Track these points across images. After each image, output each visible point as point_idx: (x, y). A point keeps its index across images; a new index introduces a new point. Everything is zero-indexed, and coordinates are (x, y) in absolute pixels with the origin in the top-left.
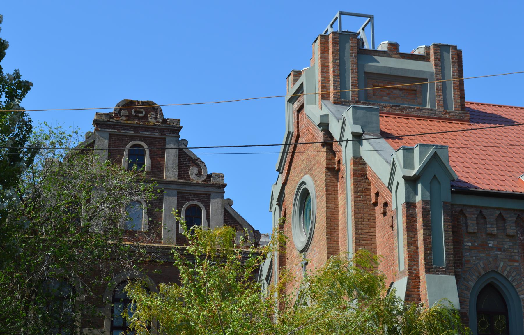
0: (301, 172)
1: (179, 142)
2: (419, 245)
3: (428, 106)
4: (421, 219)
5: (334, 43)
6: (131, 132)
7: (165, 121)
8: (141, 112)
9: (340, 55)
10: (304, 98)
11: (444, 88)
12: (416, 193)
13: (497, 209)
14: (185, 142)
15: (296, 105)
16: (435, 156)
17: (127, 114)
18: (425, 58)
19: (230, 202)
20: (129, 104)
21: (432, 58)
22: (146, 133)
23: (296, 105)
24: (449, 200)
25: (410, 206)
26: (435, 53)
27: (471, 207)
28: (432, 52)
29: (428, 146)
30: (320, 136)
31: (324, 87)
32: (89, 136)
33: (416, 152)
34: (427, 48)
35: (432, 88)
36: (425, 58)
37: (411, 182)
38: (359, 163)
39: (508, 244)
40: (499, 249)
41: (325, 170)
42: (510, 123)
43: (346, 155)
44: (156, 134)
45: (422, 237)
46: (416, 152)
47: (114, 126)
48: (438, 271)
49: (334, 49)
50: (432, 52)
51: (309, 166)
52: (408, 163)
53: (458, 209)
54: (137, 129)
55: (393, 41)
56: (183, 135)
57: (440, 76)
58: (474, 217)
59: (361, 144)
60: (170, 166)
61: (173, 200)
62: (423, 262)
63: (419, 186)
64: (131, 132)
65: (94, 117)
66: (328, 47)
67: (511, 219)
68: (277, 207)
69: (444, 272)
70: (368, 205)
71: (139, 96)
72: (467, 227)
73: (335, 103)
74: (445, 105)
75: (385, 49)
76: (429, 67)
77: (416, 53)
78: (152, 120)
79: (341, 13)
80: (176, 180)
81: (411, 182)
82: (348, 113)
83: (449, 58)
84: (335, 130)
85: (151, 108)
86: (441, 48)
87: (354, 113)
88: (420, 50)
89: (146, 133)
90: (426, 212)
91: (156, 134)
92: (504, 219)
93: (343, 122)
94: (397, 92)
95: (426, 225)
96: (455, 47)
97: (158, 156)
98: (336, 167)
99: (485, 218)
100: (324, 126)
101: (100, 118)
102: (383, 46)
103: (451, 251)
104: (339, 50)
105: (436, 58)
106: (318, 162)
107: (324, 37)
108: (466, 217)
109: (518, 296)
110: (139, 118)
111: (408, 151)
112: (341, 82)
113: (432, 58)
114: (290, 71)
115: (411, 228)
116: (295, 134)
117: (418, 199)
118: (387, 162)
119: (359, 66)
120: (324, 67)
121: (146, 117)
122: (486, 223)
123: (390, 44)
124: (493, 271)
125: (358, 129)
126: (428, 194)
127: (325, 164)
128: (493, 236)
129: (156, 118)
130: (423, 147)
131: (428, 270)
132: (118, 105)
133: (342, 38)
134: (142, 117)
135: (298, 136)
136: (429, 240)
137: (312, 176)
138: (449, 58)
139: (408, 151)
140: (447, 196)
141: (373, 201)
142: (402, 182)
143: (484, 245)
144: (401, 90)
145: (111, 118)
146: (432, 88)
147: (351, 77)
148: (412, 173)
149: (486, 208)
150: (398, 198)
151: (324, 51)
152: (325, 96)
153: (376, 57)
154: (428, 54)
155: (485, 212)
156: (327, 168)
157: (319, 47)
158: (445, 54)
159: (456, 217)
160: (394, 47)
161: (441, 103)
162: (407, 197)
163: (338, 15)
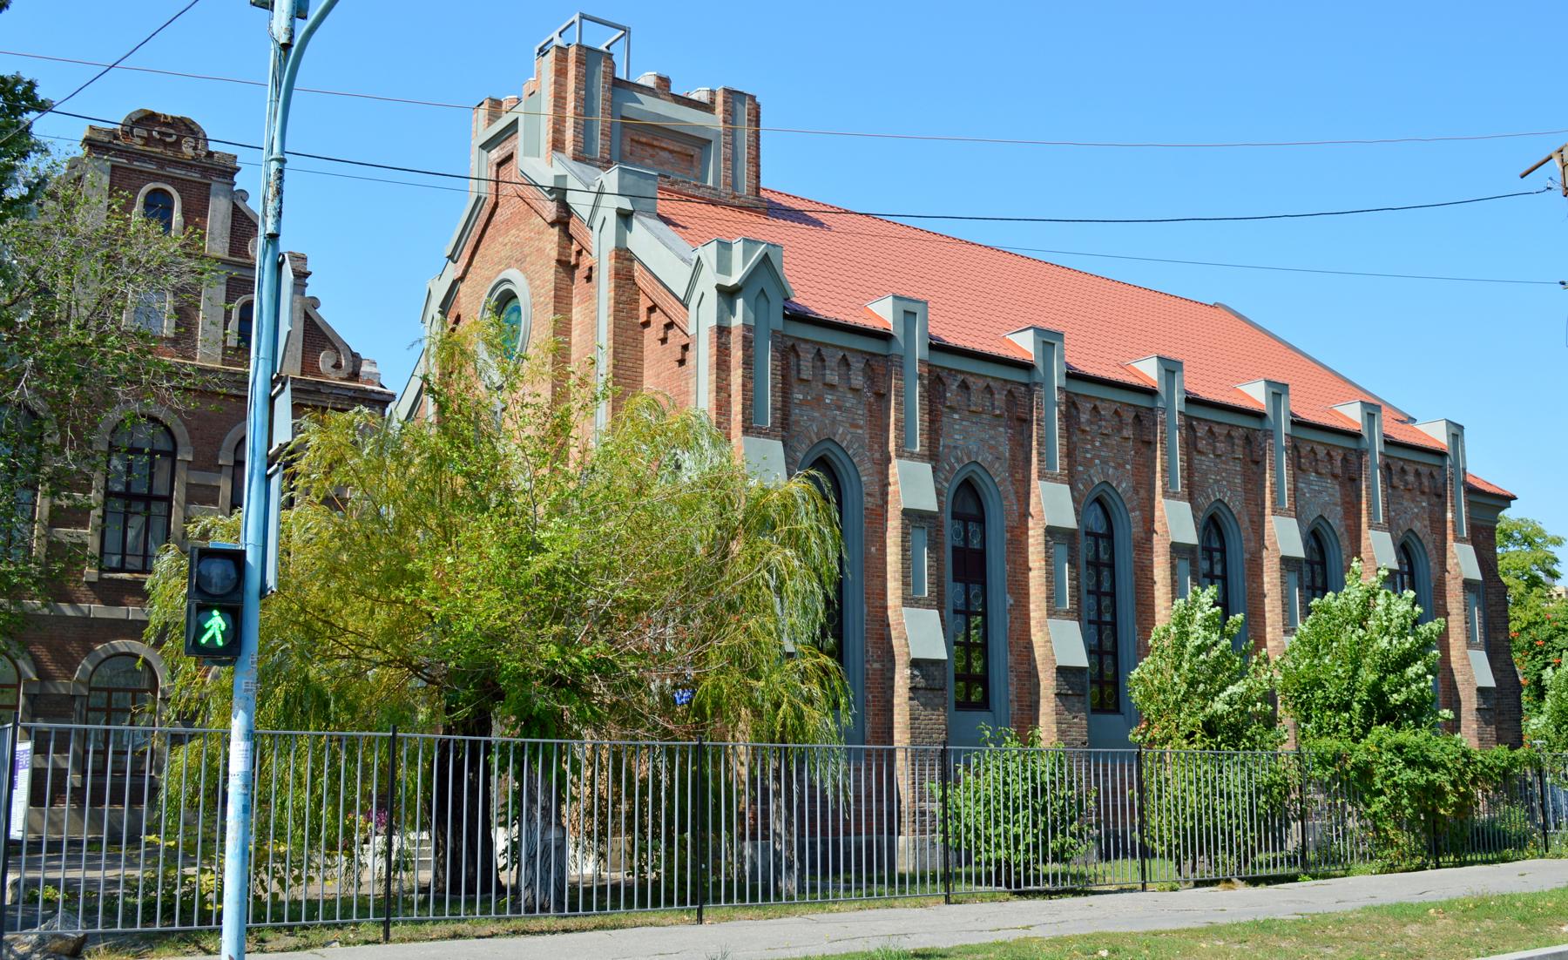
0: (500, 263)
1: (233, 193)
2: (733, 392)
3: (710, 183)
4: (740, 353)
5: (579, 62)
6: (151, 167)
7: (210, 154)
8: (170, 135)
9: (585, 81)
10: (519, 143)
11: (733, 159)
12: (733, 312)
13: (841, 348)
14: (244, 195)
15: (496, 154)
16: (765, 259)
17: (145, 134)
18: (707, 107)
19: (315, 303)
20: (148, 119)
21: (719, 109)
22: (179, 173)
23: (496, 154)
24: (780, 328)
25: (722, 331)
26: (725, 102)
27: (806, 341)
28: (720, 99)
29: (757, 242)
30: (551, 210)
31: (558, 131)
32: (74, 164)
33: (738, 249)
34: (713, 92)
35: (717, 155)
36: (707, 107)
37: (727, 294)
38: (624, 256)
39: (850, 401)
40: (839, 408)
41: (554, 263)
42: (821, 225)
43: (600, 245)
44: (195, 176)
45: (740, 380)
46: (738, 249)
47: (121, 152)
48: (760, 433)
49: (578, 72)
50: (720, 99)
51: (517, 255)
52: (724, 267)
53: (790, 343)
54: (162, 162)
55: (664, 74)
56: (241, 181)
57: (729, 139)
58: (810, 356)
59: (628, 226)
60: (217, 232)
61: (220, 291)
62: (740, 417)
63: (740, 303)
64: (151, 167)
65: (85, 133)
66: (566, 67)
67: (857, 364)
68: (438, 316)
69: (767, 434)
70: (635, 325)
71: (168, 108)
72: (799, 372)
73: (575, 159)
74: (735, 185)
75: (652, 85)
76: (714, 122)
77: (694, 96)
78: (187, 150)
79: (583, 17)
80: (226, 257)
81: (727, 294)
82: (611, 179)
83: (744, 111)
84: (580, 202)
85: (186, 127)
86: (733, 95)
87: (621, 179)
88: (701, 95)
89: (179, 173)
90: (747, 343)
91: (195, 176)
92: (848, 365)
93: (598, 194)
94: (665, 155)
95: (747, 363)
96: (753, 98)
97: (196, 212)
98: (573, 261)
99: (823, 360)
100: (559, 193)
101: (95, 136)
102: (647, 79)
103: (779, 405)
104: (585, 75)
105: (725, 111)
106: (540, 250)
107: (562, 52)
108: (798, 356)
109: (859, 477)
110: (166, 145)
111: (724, 247)
112: (585, 129)
113: (719, 109)
114: (484, 97)
115: (722, 365)
116: (491, 200)
117: (737, 321)
118: (684, 260)
119: (614, 108)
120: (559, 100)
121: (178, 143)
122: (824, 368)
123: (659, 78)
124: (829, 439)
125: (626, 204)
126: (751, 316)
127: (554, 254)
128: (832, 387)
129: (195, 148)
130: (750, 243)
131: (747, 430)
132: (129, 117)
133: (589, 57)
134: (171, 144)
135: (496, 205)
136: (749, 386)
137: (523, 270)
138: (744, 111)
139: (724, 247)
140: (777, 322)
141: (643, 318)
142: (712, 297)
143: (819, 400)
144: (671, 152)
145: (116, 138)
146: (717, 155)
147: (600, 120)
148: (733, 280)
149: (826, 345)
150: (703, 318)
151: (561, 72)
152: (558, 145)
153: (639, 96)
154: (713, 102)
155: (824, 351)
156: (558, 261)
157: (553, 66)
158: (739, 106)
159: (788, 352)
160: (664, 82)
161: (729, 180)
162: (720, 318)
163: (576, 18)
